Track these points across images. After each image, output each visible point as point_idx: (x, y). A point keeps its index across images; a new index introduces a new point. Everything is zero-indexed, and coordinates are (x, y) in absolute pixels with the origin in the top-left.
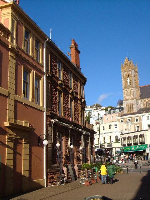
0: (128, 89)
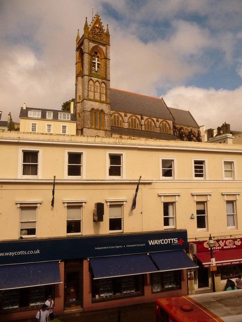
0: (97, 79)
